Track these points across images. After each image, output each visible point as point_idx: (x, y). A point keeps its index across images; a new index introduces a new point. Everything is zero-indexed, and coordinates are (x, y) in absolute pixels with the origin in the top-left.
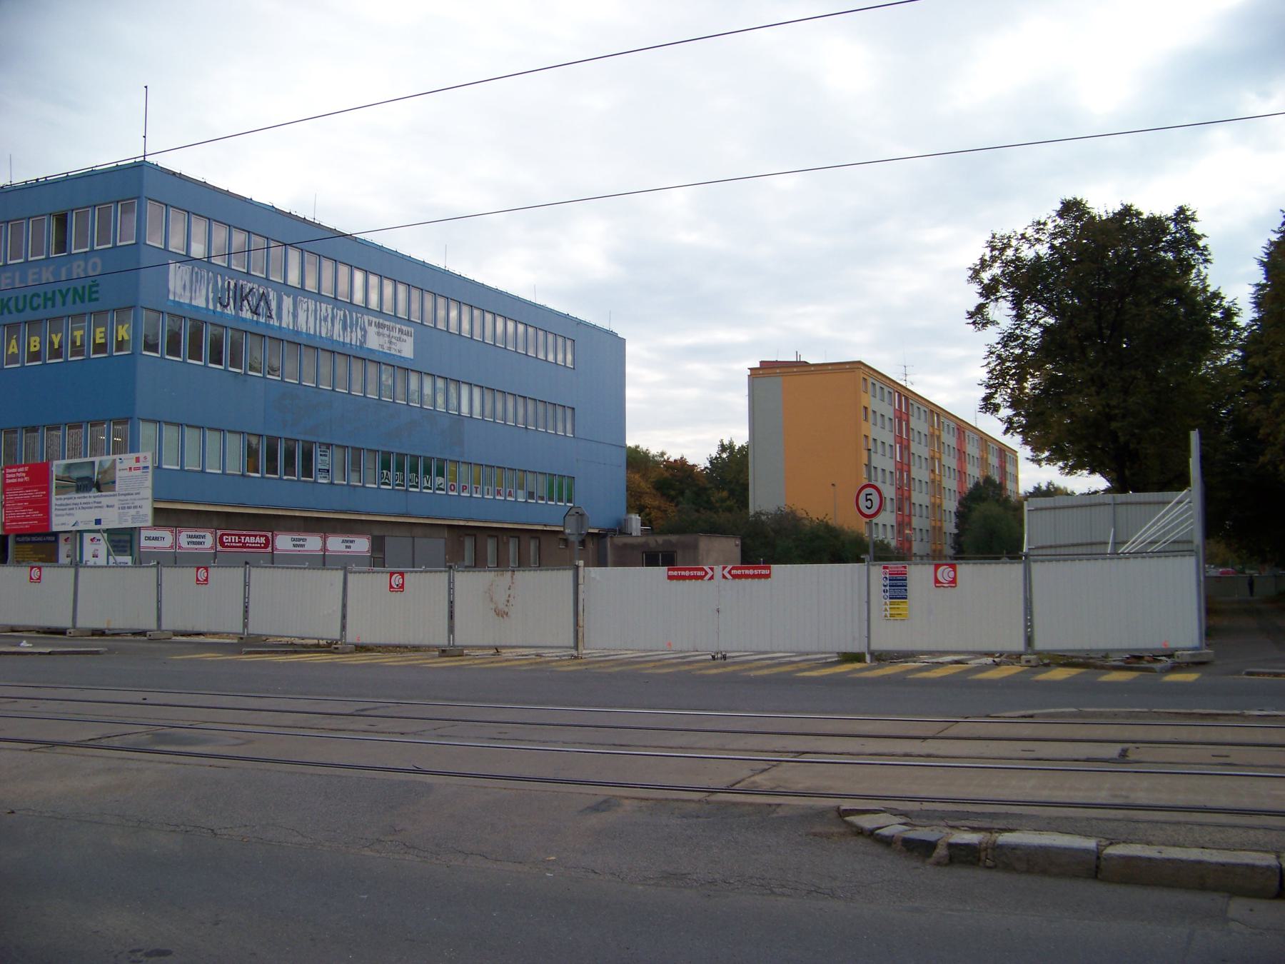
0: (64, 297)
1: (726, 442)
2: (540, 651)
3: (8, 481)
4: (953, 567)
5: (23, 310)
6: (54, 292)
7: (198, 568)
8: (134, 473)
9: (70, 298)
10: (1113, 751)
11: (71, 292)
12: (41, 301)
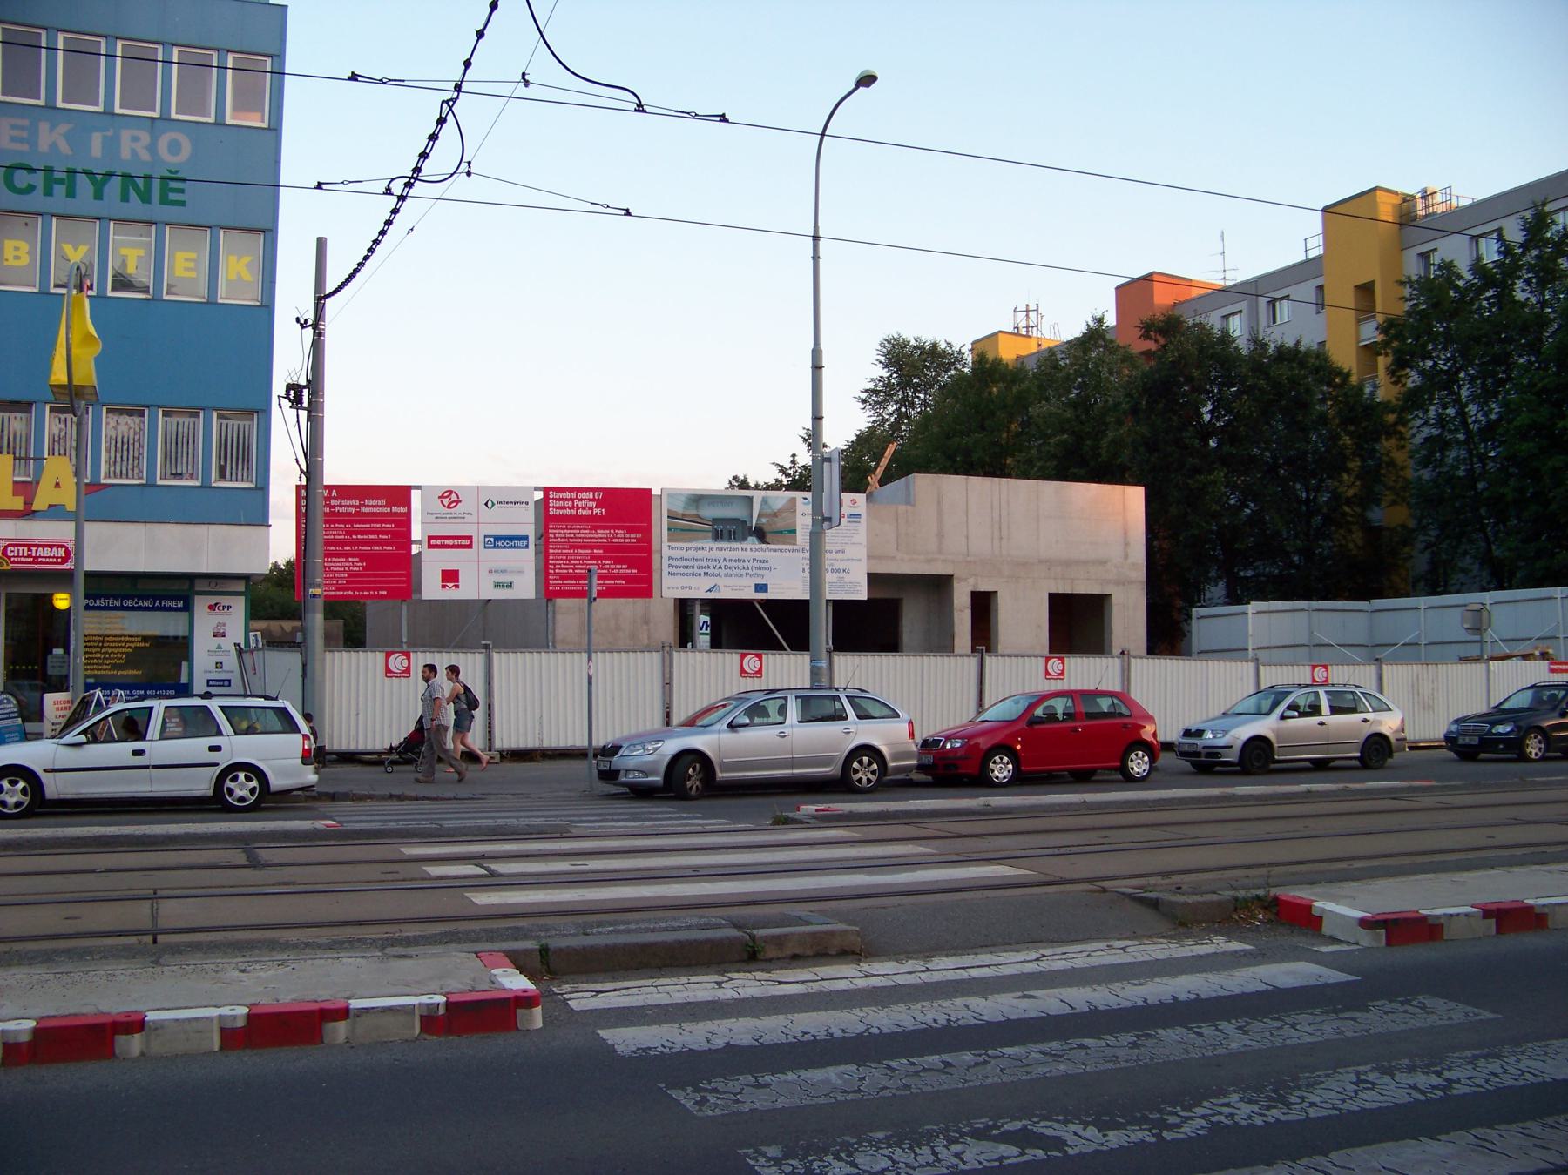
3: (552, 512)
4: (407, 655)
7: (1314, 667)
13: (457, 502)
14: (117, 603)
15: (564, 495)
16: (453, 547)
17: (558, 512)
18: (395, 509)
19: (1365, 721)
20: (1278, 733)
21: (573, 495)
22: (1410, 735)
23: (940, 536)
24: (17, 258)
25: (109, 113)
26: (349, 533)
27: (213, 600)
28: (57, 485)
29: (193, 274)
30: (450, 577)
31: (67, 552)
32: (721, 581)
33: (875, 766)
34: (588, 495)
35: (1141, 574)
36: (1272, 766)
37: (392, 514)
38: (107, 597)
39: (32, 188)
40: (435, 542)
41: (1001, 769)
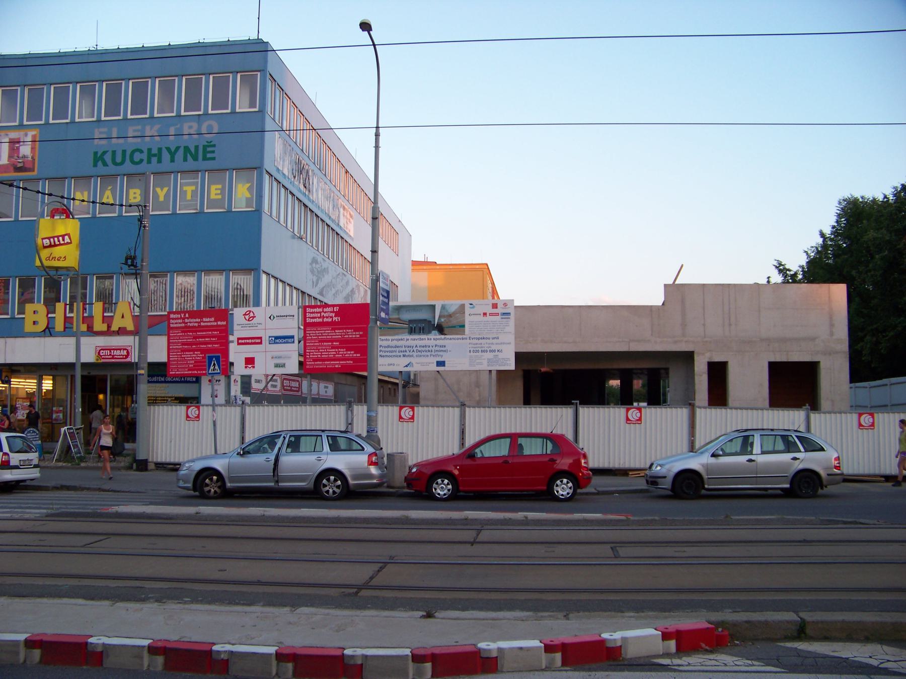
0: (173, 154)
3: (308, 320)
4: (872, 415)
5: (123, 163)
8: (488, 318)
9: (180, 155)
10: (485, 535)
11: (182, 150)
12: (144, 156)
13: (254, 317)
14: (163, 379)
15: (315, 310)
16: (252, 344)
17: (312, 320)
18: (219, 323)
19: (795, 459)
20: (707, 467)
21: (321, 310)
22: (848, 469)
23: (684, 325)
24: (135, 198)
25: (179, 116)
26: (195, 338)
28: (123, 317)
29: (220, 197)
30: (250, 361)
31: (128, 352)
32: (414, 360)
33: (339, 483)
34: (330, 309)
35: (845, 346)
36: (703, 492)
37: (217, 326)
38: (158, 376)
39: (142, 161)
40: (242, 341)
41: (442, 488)
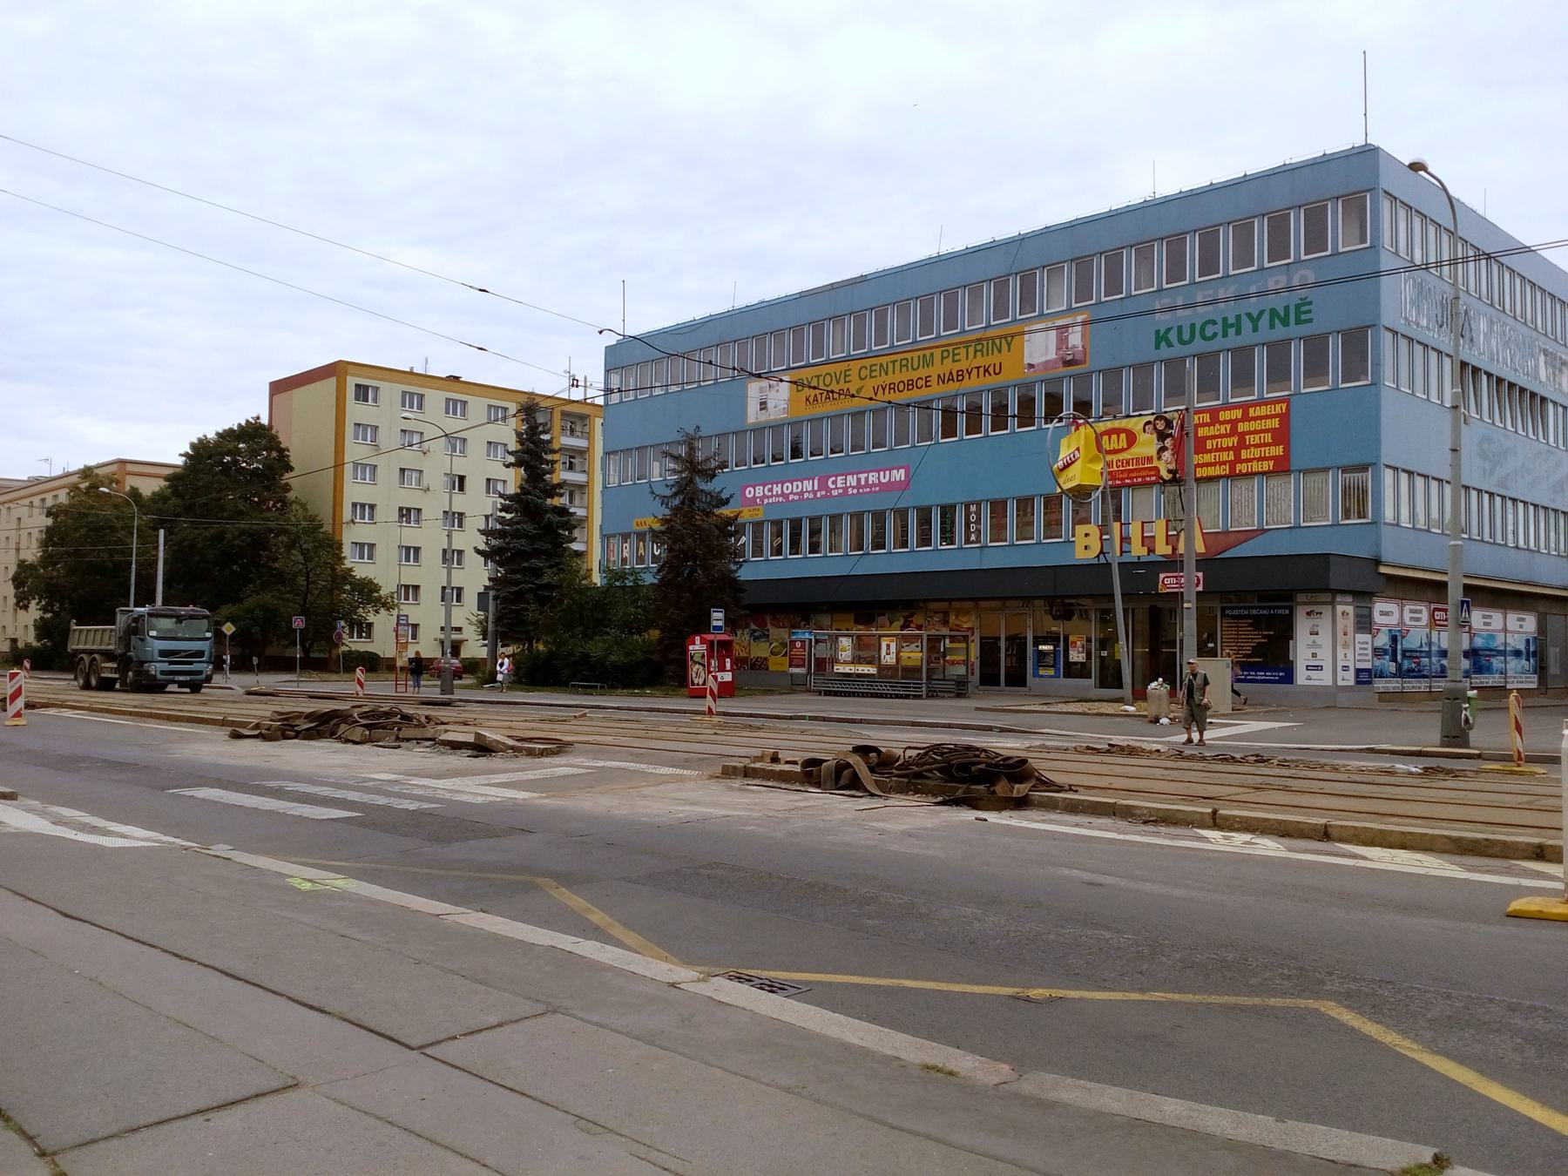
1: (24, 625)
2: (1045, 708)
6: (1238, 317)
9: (1264, 322)
11: (1266, 316)
12: (1219, 328)
27: (1309, 608)
39: (1215, 334)
41: (1104, 654)
